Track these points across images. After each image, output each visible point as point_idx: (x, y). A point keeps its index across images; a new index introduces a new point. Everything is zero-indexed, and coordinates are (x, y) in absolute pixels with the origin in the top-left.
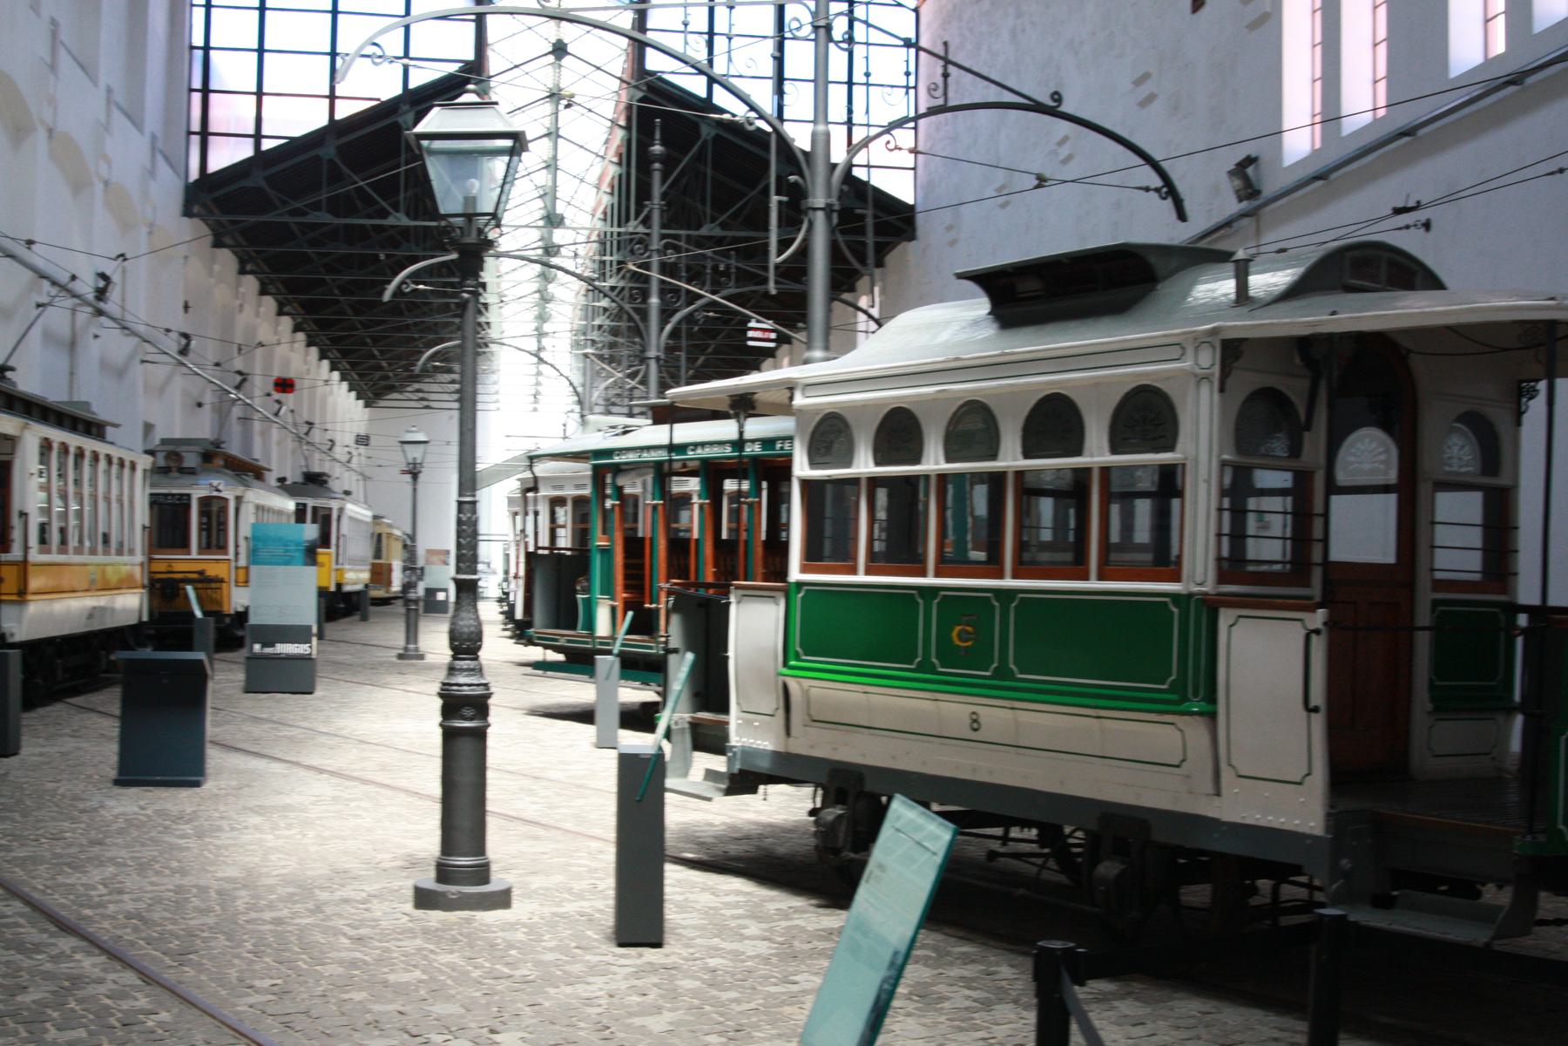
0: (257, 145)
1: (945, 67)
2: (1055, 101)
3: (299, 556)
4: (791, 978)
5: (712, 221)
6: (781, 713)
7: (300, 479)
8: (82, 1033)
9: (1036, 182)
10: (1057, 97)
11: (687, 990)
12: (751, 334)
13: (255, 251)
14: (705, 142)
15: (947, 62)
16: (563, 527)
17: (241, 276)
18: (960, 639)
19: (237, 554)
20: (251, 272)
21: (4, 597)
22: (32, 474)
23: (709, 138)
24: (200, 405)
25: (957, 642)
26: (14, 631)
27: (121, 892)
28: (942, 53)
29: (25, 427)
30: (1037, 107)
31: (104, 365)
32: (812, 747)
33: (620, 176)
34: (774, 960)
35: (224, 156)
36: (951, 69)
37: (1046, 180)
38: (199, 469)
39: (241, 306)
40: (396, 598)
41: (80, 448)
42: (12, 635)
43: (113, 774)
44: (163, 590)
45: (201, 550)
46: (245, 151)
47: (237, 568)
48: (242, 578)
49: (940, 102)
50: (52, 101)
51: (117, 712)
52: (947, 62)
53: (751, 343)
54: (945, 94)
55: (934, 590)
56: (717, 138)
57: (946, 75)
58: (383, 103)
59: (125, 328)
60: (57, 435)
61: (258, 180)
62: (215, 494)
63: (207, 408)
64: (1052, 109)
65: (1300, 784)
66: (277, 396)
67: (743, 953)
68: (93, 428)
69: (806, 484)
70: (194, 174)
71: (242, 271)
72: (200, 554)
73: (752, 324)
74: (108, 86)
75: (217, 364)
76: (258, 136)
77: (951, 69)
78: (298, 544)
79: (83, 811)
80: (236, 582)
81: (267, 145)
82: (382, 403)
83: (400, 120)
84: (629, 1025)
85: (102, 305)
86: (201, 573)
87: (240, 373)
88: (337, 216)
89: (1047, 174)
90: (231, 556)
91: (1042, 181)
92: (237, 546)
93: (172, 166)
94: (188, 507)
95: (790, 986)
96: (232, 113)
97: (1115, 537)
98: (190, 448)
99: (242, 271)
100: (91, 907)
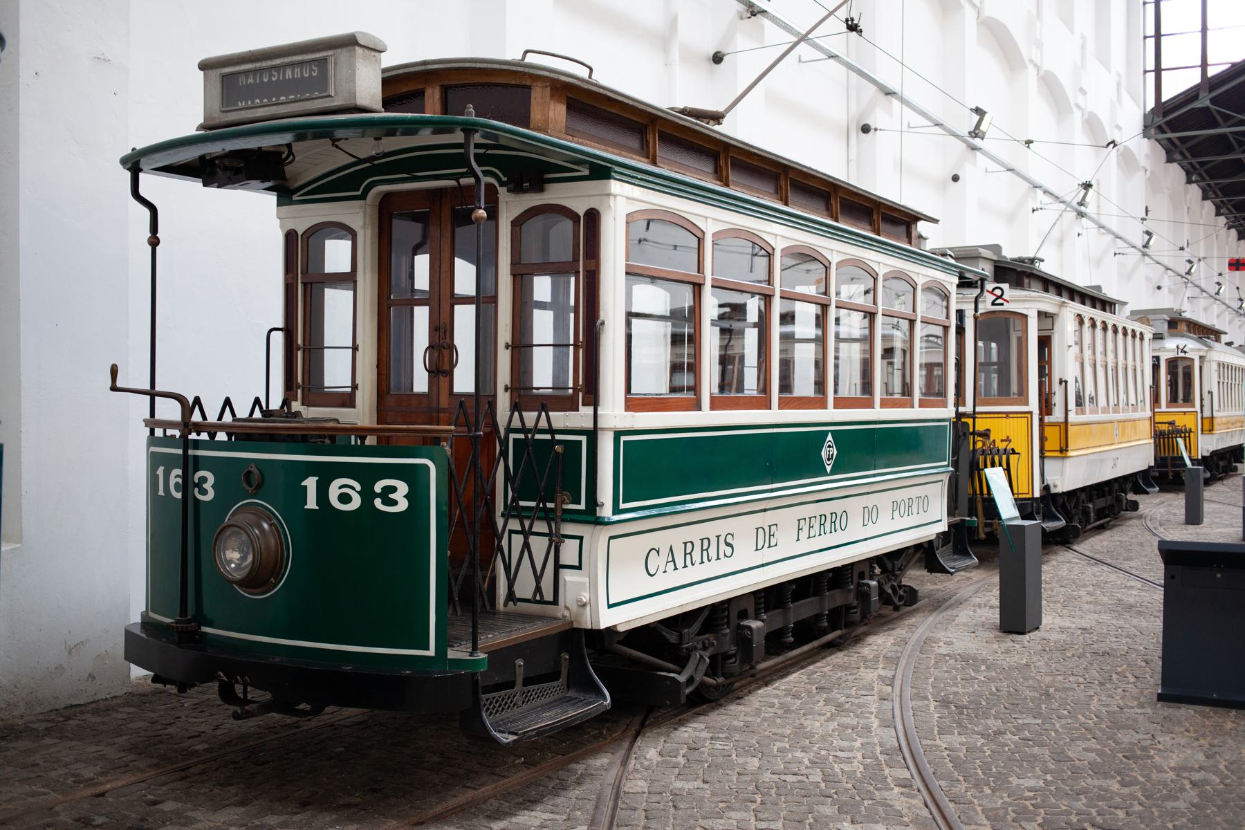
8: (994, 674)
13: (1198, 163)
17: (1188, 185)
19: (1202, 406)
20: (1196, 182)
22: (1070, 346)
24: (1159, 288)
26: (1058, 483)
29: (1063, 304)
35: (1174, 86)
38: (1166, 334)
42: (1055, 486)
44: (1164, 437)
46: (1192, 79)
47: (1202, 418)
48: (1206, 427)
50: (1039, 44)
59: (1103, 227)
60: (1088, 311)
61: (1204, 102)
63: (1165, 290)
68: (1106, 304)
70: (1151, 104)
71: (1189, 181)
72: (1167, 407)
74: (1082, 34)
76: (1204, 65)
80: (1202, 430)
81: (1211, 72)
85: (1083, 209)
90: (1198, 408)
92: (1202, 399)
93: (1134, 100)
97: (981, 359)
99: (1189, 181)
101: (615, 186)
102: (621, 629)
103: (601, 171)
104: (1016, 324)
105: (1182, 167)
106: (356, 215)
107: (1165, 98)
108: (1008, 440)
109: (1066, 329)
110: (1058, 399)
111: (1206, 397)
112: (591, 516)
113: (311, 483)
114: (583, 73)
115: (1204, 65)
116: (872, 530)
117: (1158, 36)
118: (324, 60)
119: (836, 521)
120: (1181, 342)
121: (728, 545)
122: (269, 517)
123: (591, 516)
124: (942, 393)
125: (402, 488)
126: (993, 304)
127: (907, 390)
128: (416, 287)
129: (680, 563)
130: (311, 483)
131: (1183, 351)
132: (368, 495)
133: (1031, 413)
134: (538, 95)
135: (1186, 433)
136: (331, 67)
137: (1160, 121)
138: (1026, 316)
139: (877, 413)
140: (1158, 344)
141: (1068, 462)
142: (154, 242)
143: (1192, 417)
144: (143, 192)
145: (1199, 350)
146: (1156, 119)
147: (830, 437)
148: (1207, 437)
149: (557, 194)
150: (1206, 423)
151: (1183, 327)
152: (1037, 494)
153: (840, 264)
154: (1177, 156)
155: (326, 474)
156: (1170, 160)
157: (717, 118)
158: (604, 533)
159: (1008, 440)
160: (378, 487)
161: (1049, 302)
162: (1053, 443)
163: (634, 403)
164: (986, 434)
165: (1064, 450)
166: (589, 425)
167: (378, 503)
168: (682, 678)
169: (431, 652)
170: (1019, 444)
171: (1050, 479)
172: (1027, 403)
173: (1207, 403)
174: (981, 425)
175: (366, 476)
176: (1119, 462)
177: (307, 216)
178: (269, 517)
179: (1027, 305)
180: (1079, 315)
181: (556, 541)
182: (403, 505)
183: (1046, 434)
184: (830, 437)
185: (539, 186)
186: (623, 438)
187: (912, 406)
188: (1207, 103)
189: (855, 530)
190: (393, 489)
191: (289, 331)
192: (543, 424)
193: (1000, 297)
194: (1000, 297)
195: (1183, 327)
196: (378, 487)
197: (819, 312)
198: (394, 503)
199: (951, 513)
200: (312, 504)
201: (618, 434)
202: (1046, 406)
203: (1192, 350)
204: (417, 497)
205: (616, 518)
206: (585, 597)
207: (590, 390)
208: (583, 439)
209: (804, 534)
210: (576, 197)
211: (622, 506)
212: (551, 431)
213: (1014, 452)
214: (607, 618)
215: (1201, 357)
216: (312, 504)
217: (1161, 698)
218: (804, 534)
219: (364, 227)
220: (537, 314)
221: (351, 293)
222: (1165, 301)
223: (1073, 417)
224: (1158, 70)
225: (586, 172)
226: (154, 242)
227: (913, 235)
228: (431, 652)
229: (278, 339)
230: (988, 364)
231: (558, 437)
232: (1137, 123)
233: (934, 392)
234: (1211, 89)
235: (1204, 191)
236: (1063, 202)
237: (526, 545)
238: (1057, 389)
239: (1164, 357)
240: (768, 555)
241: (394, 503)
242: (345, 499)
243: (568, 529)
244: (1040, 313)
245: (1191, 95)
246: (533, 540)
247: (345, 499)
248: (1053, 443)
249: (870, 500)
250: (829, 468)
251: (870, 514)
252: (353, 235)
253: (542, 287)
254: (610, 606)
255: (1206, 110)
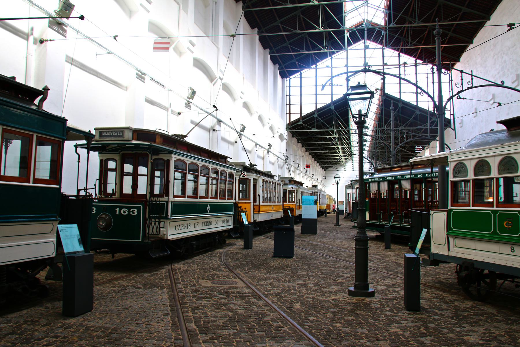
0: (301, 115)
1: (472, 77)
2: (502, 83)
3: (313, 203)
4: (462, 325)
5: (402, 126)
6: (446, 244)
7: (311, 186)
9: (498, 105)
10: (503, 82)
11: (432, 328)
12: (416, 149)
14: (400, 108)
15: (472, 75)
16: (113, 257)
18: (506, 225)
19: (297, 203)
21: (124, 174)
23: (401, 107)
25: (505, 226)
26: (257, 219)
27: (274, 287)
28: (471, 74)
30: (497, 85)
31: (270, 162)
32: (506, 264)
33: (380, 117)
34: (454, 318)
35: (294, 117)
36: (473, 77)
37: (501, 104)
38: (288, 184)
39: (298, 150)
40: (331, 212)
41: (266, 180)
43: (272, 254)
45: (435, 45)
46: (298, 116)
47: (297, 206)
48: (298, 208)
49: (471, 86)
51: (274, 238)
52: (472, 75)
53: (416, 152)
54: (472, 83)
55: (497, 211)
56: (402, 107)
57: (472, 79)
58: (327, 104)
60: (265, 178)
61: (316, 115)
62: (292, 189)
64: (502, 86)
65: (444, 245)
66: (306, 169)
67: (444, 315)
69: (452, 182)
70: (288, 122)
71: (298, 142)
73: (416, 147)
75: (294, 161)
76: (301, 113)
77: (473, 77)
78: (313, 201)
79: (266, 264)
81: (303, 115)
82: (328, 170)
83: (331, 108)
84: (419, 340)
86: (289, 207)
87: (298, 164)
88: (318, 129)
89: (501, 103)
90: (296, 203)
91: (499, 104)
94: (286, 192)
95: (463, 328)
96: (295, 109)
98: (287, 179)
99: (298, 142)
100: (267, 291)
101: (173, 155)
102: (171, 240)
103: (171, 152)
104: (248, 181)
105: (296, 138)
106: (117, 157)
107: (291, 121)
108: (246, 209)
109: (260, 183)
110: (258, 199)
111: (298, 200)
112: (167, 218)
113: (118, 210)
114: (166, 133)
115: (301, 113)
116: (217, 226)
117: (290, 104)
118: (122, 131)
119: (209, 223)
120: (292, 186)
121: (190, 226)
122: (108, 216)
123: (167, 218)
124: (232, 197)
125: (136, 210)
126: (243, 176)
127: (225, 196)
128: (125, 171)
129: (181, 229)
130: (118, 210)
131: (292, 188)
132: (129, 212)
133: (251, 202)
134: (157, 136)
135: (292, 209)
136: (124, 132)
137: (290, 127)
138: (250, 179)
139: (218, 200)
140: (286, 186)
141: (260, 214)
142: (79, 162)
143: (294, 205)
144: (78, 152)
145: (296, 188)
146: (289, 126)
147: (209, 205)
148: (298, 211)
149: (161, 156)
150: (298, 207)
151: (292, 182)
152: (252, 222)
153: (212, 169)
154: (295, 136)
155: (121, 208)
156: (293, 137)
157: (185, 136)
158: (168, 221)
159: (246, 209)
160: (131, 210)
161: (255, 176)
162: (256, 210)
163: (175, 197)
164: (241, 207)
165: (259, 211)
166: (167, 200)
167: (131, 213)
168: (181, 251)
169: (141, 240)
170: (248, 210)
171: (256, 218)
172: (250, 200)
173: (298, 202)
174: (240, 205)
175: (129, 208)
176: (273, 215)
177: (105, 157)
178: (108, 216)
179: (251, 177)
180: (263, 179)
181: (160, 222)
182: (136, 214)
183: (255, 208)
184: (209, 205)
185: (158, 155)
186: (173, 203)
187: (225, 199)
188: (301, 123)
189: (213, 225)
190: (134, 211)
191: (100, 180)
192: (154, 200)
193: (244, 175)
194: (244, 175)
195: (292, 182)
196: (131, 210)
197: (207, 179)
198: (134, 213)
199: (233, 224)
200: (118, 213)
201: (172, 202)
202: (255, 201)
203: (294, 188)
204: (139, 212)
205: (171, 218)
206: (165, 233)
207: (167, 194)
208: (165, 203)
209: (203, 225)
210: (165, 157)
211: (172, 216)
212: (160, 201)
213: (247, 212)
214: (169, 237)
215: (297, 190)
216: (118, 213)
217: (273, 257)
218: (203, 225)
219: (119, 160)
220: (156, 178)
221: (115, 173)
222: (287, 175)
223: (261, 204)
224: (290, 113)
225: (167, 152)
226: (79, 162)
227: (226, 161)
228: (141, 240)
229: (98, 181)
230: (243, 190)
231: (161, 203)
232: (284, 127)
233: (230, 197)
234: (303, 119)
235: (302, 145)
236: (264, 148)
237: (155, 223)
238: (257, 197)
239: (288, 190)
240: (217, 226)
241: (134, 213)
242: (125, 212)
243: (161, 220)
244: (254, 179)
245: (297, 121)
246: (156, 222)
247: (125, 212)
248: (256, 210)
249: (217, 219)
250: (208, 212)
251: (216, 222)
252: (116, 161)
253: (157, 173)
254: (169, 235)
255: (301, 125)
